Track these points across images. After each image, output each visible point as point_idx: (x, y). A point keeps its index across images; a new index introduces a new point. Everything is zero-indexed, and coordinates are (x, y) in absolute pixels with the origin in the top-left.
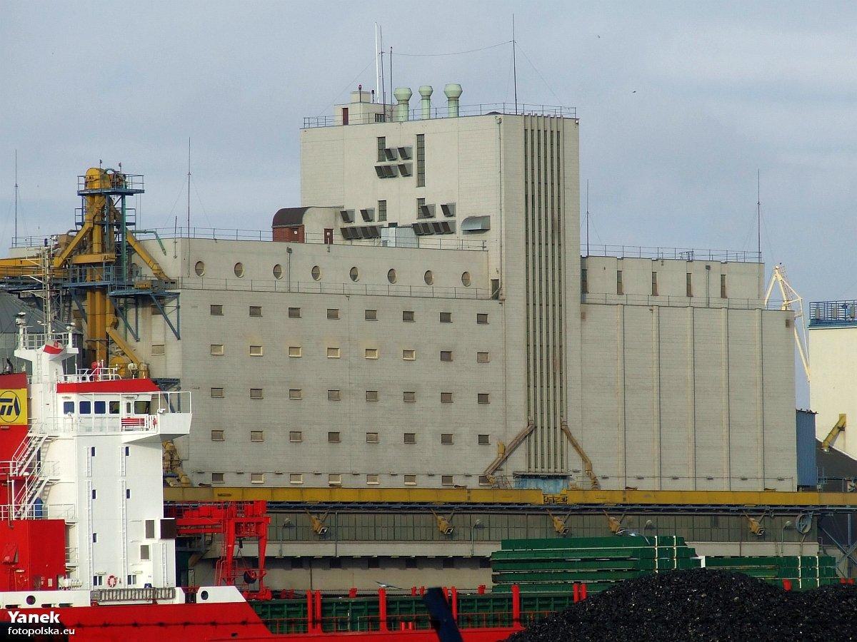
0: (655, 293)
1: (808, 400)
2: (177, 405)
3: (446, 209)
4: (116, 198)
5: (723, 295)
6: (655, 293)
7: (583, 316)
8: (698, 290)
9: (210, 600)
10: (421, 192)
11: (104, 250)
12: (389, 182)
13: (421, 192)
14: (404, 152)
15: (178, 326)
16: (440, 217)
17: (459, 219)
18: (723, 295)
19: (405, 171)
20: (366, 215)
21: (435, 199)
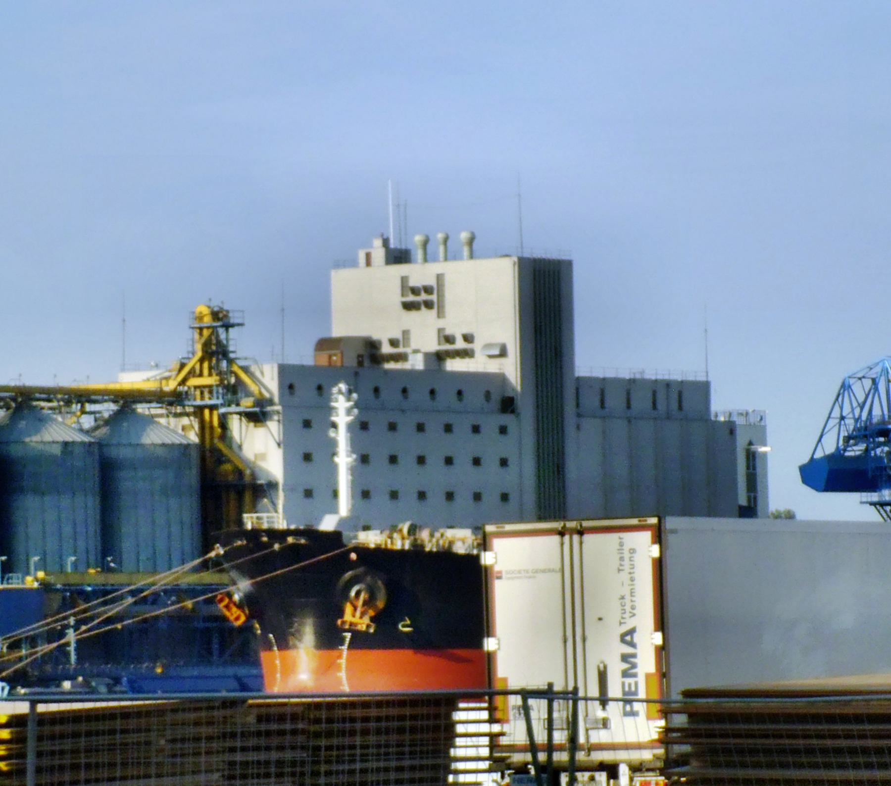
0: (629, 407)
1: (648, 708)
2: (830, 428)
3: (468, 338)
4: (221, 331)
5: (680, 408)
6: (629, 407)
7: (578, 427)
8: (661, 406)
9: (637, 519)
10: (441, 323)
11: (210, 375)
12: (414, 314)
13: (441, 323)
14: (428, 290)
15: (829, 431)
16: (460, 344)
17: (477, 346)
18: (680, 408)
19: (429, 305)
20: (394, 343)
21: (457, 330)
